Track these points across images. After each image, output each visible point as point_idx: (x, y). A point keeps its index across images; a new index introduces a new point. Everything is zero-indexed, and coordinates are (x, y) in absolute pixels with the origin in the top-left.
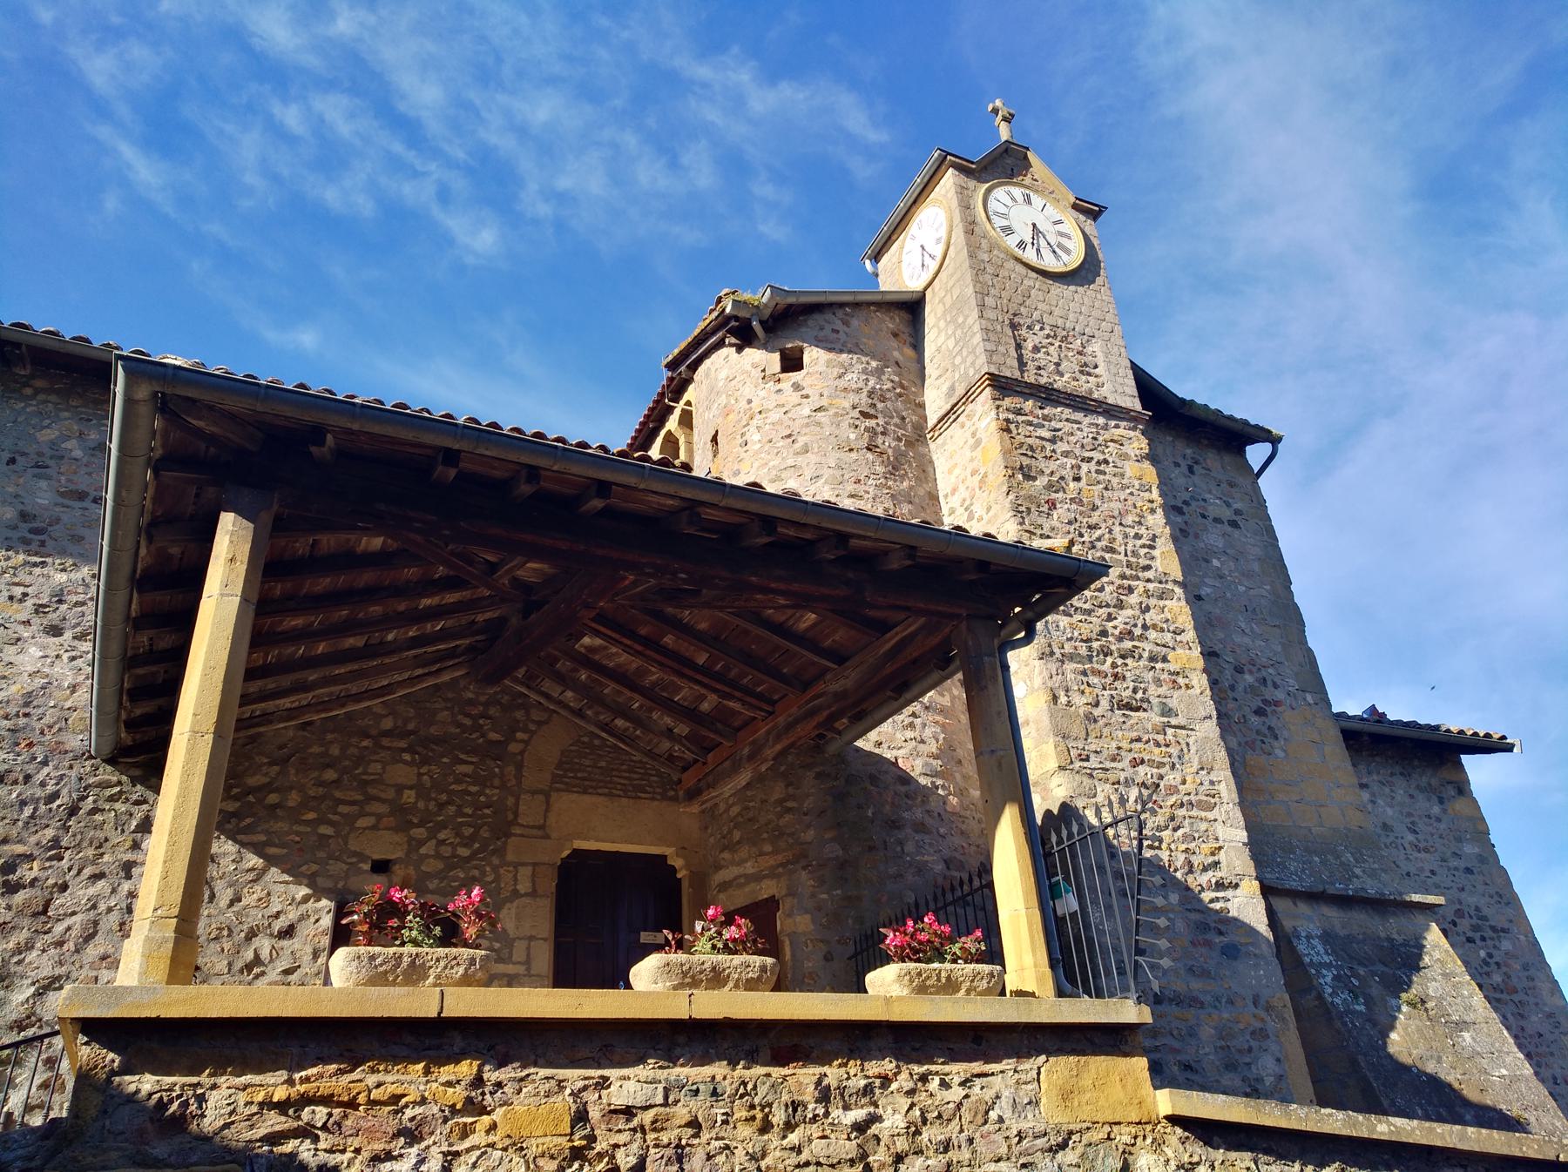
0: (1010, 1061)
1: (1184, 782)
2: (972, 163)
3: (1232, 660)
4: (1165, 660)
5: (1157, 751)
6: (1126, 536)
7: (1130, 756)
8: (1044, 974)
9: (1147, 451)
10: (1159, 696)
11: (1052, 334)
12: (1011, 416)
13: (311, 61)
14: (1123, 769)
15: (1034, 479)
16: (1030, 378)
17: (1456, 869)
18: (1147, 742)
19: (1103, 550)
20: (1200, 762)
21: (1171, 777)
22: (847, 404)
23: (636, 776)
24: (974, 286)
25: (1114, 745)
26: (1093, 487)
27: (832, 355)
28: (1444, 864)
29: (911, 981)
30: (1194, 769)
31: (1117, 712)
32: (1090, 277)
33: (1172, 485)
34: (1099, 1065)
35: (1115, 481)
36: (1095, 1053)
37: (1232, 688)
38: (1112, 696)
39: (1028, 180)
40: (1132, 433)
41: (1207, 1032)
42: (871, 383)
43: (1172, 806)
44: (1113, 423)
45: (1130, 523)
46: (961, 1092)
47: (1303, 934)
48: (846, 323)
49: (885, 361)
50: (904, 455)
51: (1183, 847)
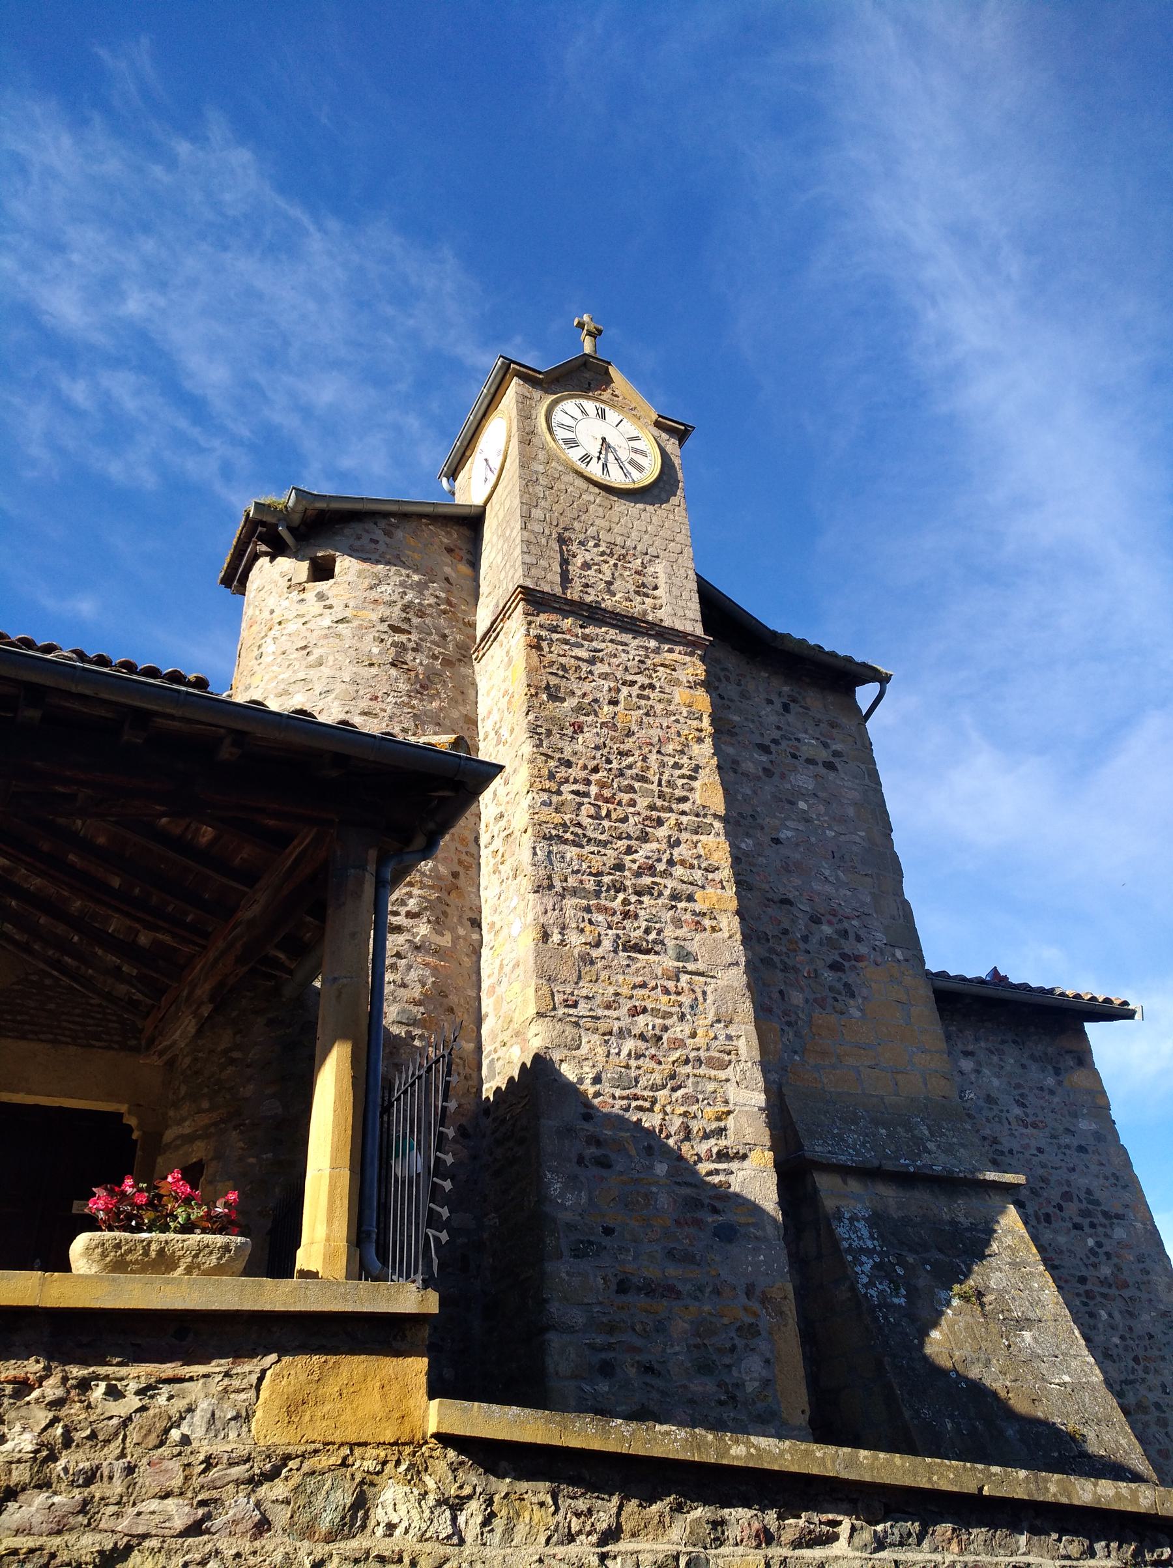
0: (223, 1361)
1: (694, 1035)
2: (540, 373)
3: (808, 909)
4: (690, 898)
5: (664, 999)
6: (663, 765)
7: (630, 1004)
8: (336, 1249)
9: (703, 678)
10: (676, 939)
11: (608, 551)
12: (544, 633)
13: (100, 339)
14: (618, 1018)
15: (563, 700)
16: (574, 594)
17: (1067, 1147)
18: (653, 989)
19: (633, 778)
20: (717, 1013)
21: (678, 1029)
22: (374, 617)
23: (91, 1022)
24: (521, 497)
25: (611, 990)
26: (632, 713)
27: (365, 566)
28: (1054, 1141)
29: (104, 1255)
30: (708, 1022)
31: (621, 953)
32: (664, 496)
33: (761, 723)
34: (354, 1366)
35: (659, 707)
36: (353, 1352)
37: (805, 939)
38: (618, 936)
39: (606, 395)
40: (688, 659)
41: (680, 1326)
42: (409, 597)
43: (674, 1063)
44: (666, 647)
45: (670, 751)
46: (136, 1402)
47: (847, 1215)
48: (388, 534)
49: (431, 575)
50: (438, 674)
51: (682, 1110)
